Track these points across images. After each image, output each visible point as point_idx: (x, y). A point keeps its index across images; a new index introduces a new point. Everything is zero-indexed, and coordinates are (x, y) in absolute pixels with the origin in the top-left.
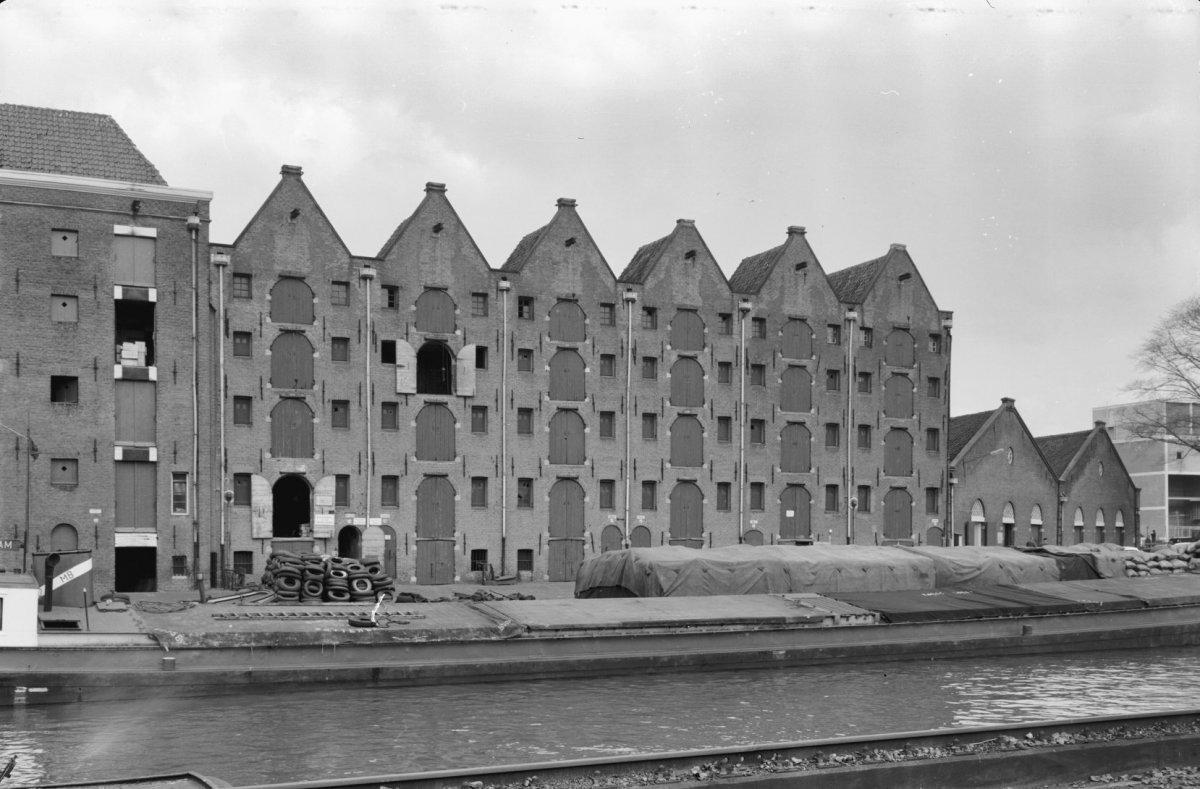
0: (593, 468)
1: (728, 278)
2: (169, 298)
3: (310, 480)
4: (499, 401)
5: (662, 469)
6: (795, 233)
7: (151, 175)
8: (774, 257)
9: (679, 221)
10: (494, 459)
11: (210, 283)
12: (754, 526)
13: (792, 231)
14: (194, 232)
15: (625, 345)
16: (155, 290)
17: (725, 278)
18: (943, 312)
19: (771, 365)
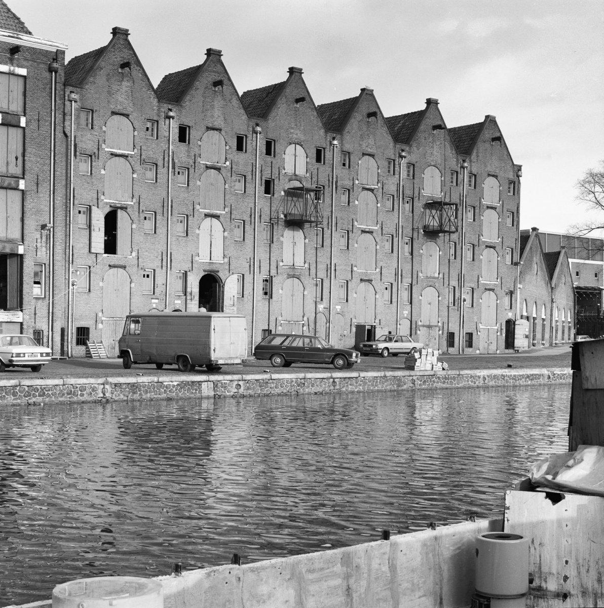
0: (309, 269)
1: (155, 87)
2: (34, 125)
3: (222, 278)
4: (253, 216)
5: (352, 271)
6: (213, 55)
7: (20, 27)
8: (192, 74)
9: (362, 90)
10: (249, 260)
11: (64, 114)
12: (406, 315)
13: (292, 71)
14: (53, 73)
15: (331, 179)
16: (25, 118)
17: (153, 88)
18: (516, 165)
19: (417, 198)
